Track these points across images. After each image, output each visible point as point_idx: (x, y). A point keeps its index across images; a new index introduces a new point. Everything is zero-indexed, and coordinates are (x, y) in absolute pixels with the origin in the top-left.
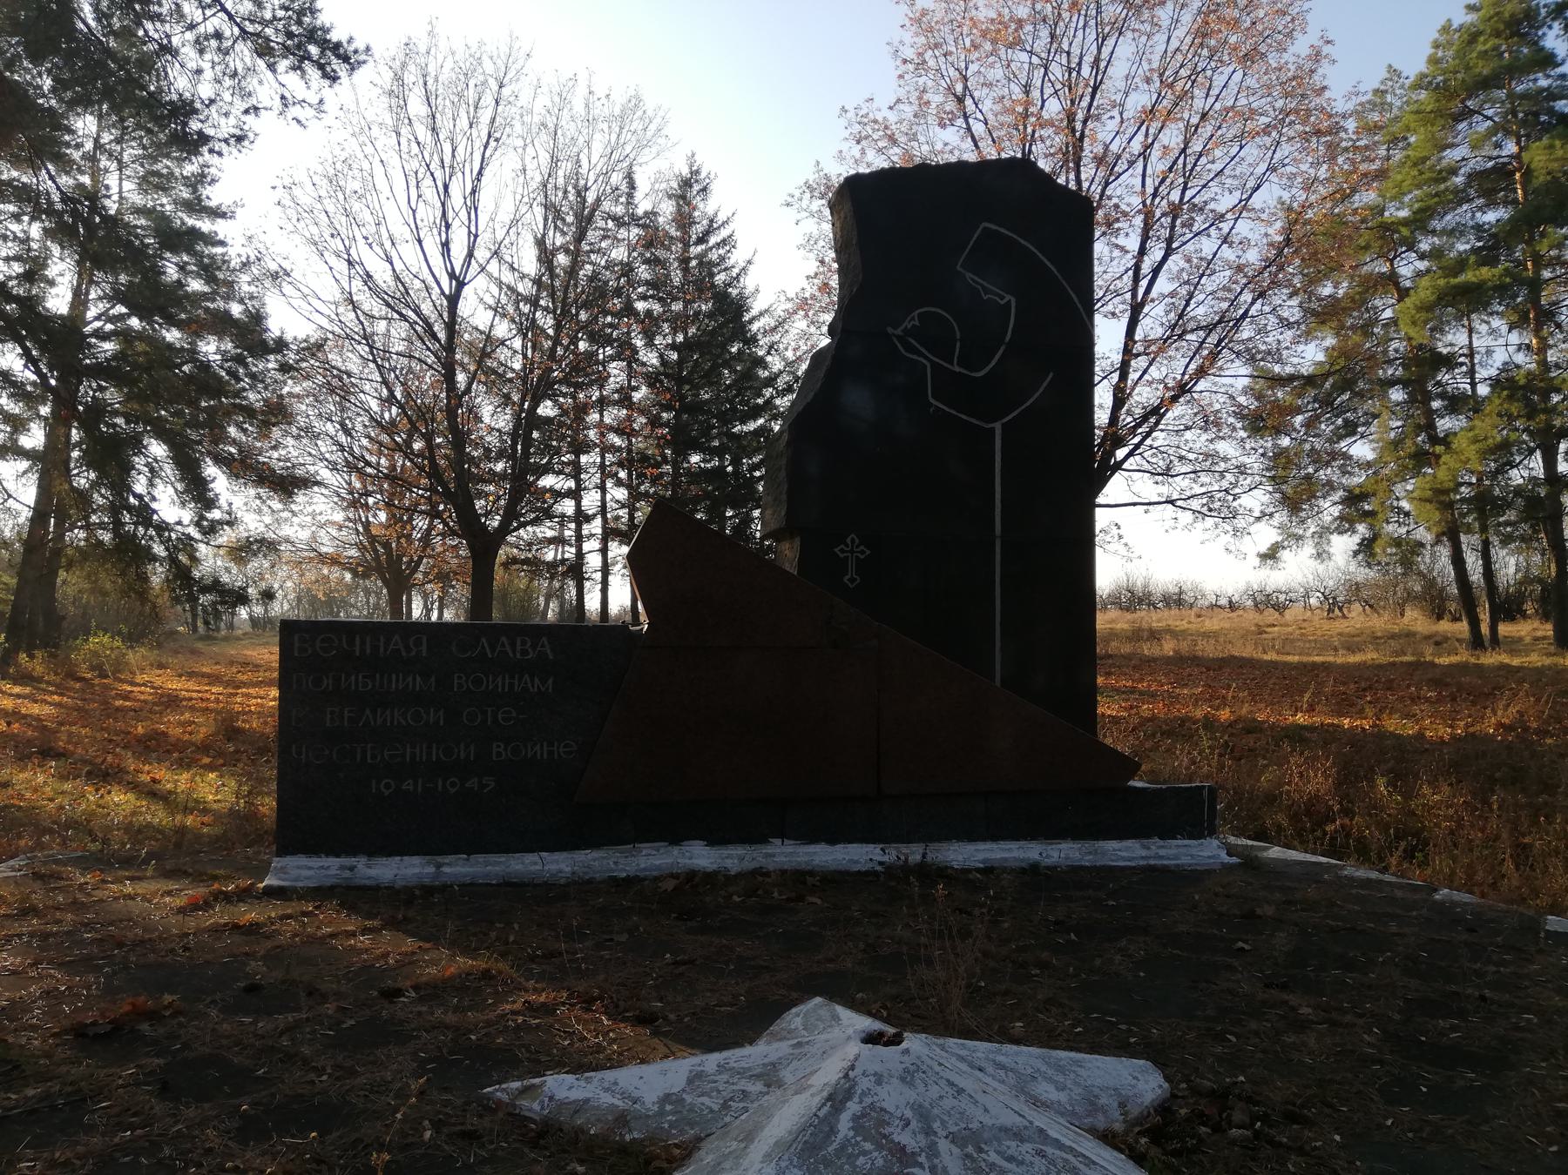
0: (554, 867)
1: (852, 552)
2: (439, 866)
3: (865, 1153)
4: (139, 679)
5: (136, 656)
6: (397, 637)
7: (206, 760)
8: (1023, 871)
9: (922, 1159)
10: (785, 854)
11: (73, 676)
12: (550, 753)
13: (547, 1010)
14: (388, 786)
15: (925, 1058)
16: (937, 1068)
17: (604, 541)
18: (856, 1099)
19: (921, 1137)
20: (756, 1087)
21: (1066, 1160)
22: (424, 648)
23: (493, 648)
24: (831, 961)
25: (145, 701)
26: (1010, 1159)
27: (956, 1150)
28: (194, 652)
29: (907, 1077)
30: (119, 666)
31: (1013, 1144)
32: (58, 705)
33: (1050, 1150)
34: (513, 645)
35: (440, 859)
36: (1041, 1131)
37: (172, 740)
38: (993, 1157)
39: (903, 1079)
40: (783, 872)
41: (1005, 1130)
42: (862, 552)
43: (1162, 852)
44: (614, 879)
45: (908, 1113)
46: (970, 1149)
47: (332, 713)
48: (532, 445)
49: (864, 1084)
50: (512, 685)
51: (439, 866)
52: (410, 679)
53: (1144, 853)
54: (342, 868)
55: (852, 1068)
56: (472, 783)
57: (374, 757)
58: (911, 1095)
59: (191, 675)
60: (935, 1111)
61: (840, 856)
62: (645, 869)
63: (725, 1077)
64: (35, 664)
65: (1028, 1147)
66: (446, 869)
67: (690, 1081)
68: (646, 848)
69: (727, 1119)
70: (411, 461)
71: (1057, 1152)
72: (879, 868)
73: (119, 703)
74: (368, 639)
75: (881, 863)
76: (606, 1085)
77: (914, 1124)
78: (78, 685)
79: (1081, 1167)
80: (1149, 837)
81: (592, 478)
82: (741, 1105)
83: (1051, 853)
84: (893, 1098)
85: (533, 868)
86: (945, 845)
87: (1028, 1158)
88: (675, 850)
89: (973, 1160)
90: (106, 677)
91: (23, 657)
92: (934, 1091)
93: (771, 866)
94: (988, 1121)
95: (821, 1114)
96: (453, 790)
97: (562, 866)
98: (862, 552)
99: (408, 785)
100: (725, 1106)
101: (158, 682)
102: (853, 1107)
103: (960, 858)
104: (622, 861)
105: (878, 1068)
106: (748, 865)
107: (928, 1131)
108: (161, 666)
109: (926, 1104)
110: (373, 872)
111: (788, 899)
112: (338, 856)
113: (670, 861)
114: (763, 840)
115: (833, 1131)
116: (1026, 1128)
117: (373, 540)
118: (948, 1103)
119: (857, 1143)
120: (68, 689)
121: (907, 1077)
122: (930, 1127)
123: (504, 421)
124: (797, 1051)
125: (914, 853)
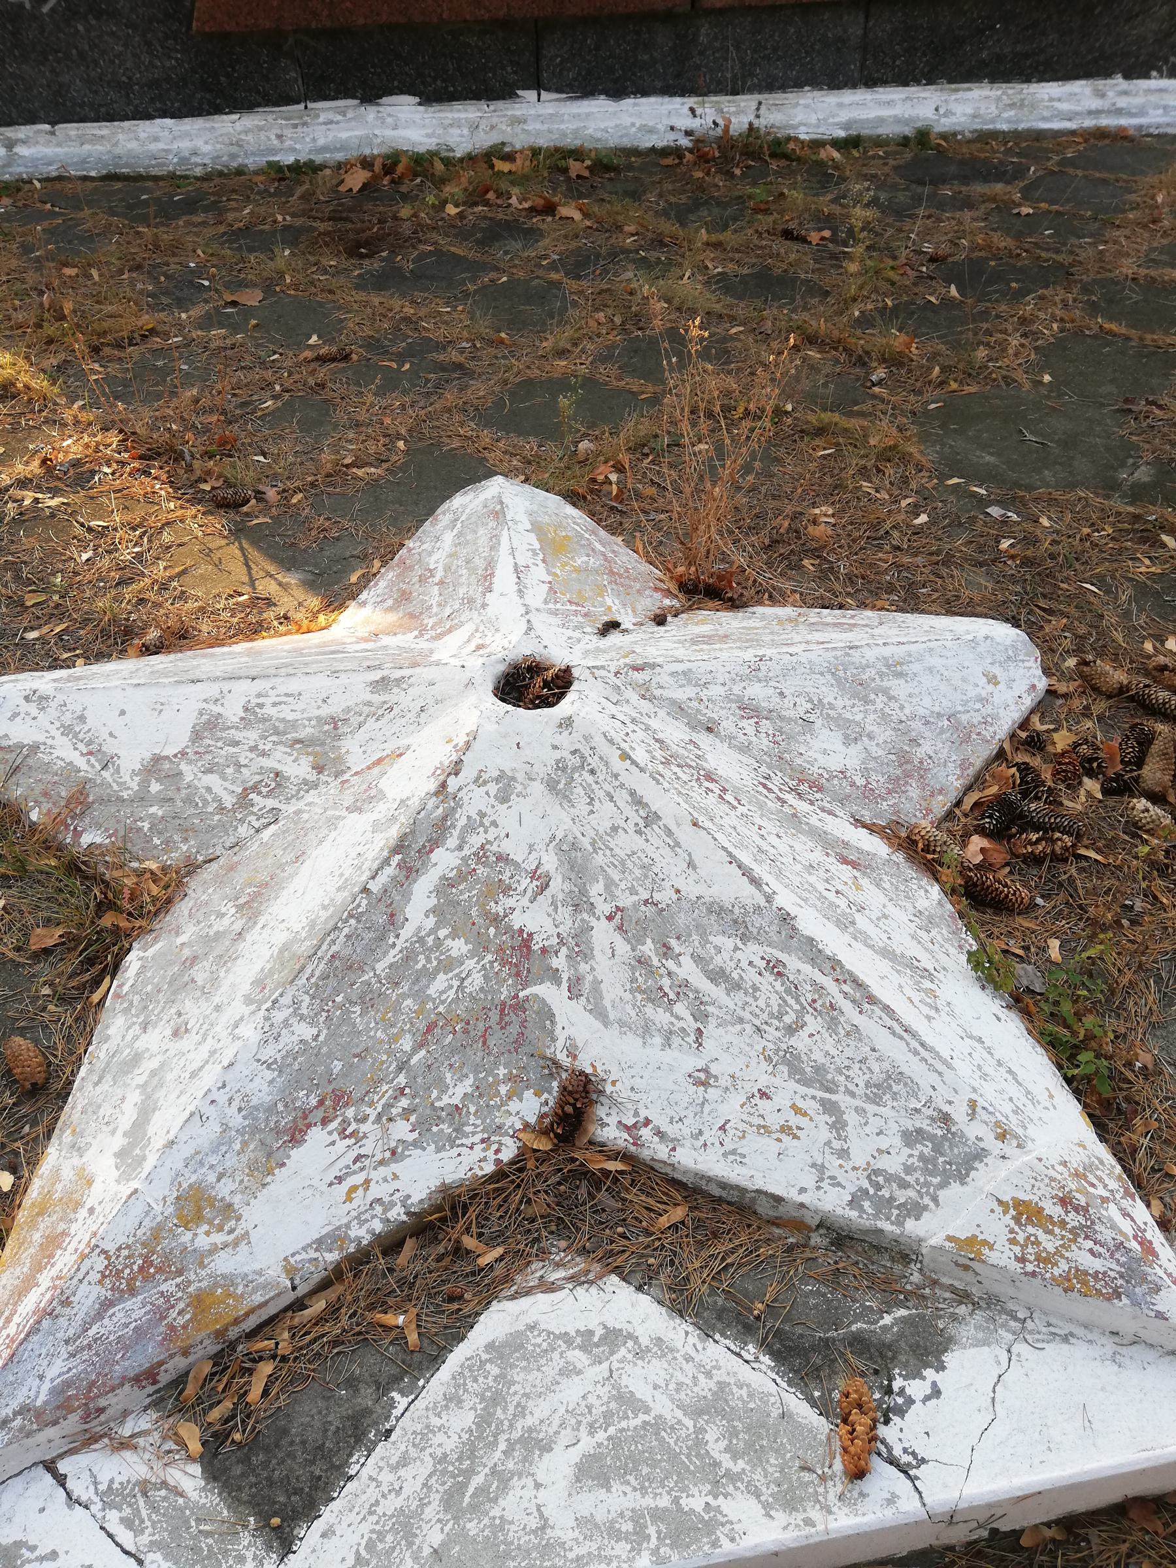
0: (185, 145)
3: (448, 965)
8: (905, 141)
9: (559, 962)
10: (545, 119)
13: (79, 475)
15: (599, 741)
16: (618, 765)
18: (452, 842)
19: (565, 913)
20: (298, 768)
21: (819, 989)
24: (562, 353)
26: (717, 976)
27: (623, 948)
29: (560, 782)
31: (728, 943)
33: (793, 963)
36: (786, 918)
38: (687, 970)
39: (551, 785)
40: (536, 152)
41: (717, 910)
43: (1122, 102)
44: (276, 167)
45: (550, 862)
46: (648, 948)
49: (475, 801)
53: (1095, 104)
55: (456, 768)
58: (561, 820)
60: (599, 859)
61: (626, 120)
62: (324, 149)
63: (251, 736)
65: (753, 952)
66: (21, 150)
67: (197, 736)
68: (325, 110)
69: (243, 831)
71: (807, 969)
72: (685, 142)
75: (688, 133)
76: (68, 719)
77: (557, 885)
79: (846, 1006)
80: (1108, 75)
82: (270, 803)
83: (954, 107)
84: (527, 829)
85: (154, 147)
86: (791, 97)
87: (751, 976)
88: (370, 113)
89: (651, 972)
92: (606, 815)
93: (519, 140)
94: (692, 890)
95: (375, 887)
97: (199, 143)
100: (243, 801)
102: (444, 860)
103: (813, 119)
104: (288, 132)
105: (506, 761)
106: (484, 140)
107: (580, 903)
109: (585, 842)
111: (532, 209)
114: (504, 92)
115: (394, 920)
116: (758, 909)
118: (626, 842)
119: (439, 942)
121: (560, 782)
122: (583, 892)
124: (376, 699)
125: (739, 112)
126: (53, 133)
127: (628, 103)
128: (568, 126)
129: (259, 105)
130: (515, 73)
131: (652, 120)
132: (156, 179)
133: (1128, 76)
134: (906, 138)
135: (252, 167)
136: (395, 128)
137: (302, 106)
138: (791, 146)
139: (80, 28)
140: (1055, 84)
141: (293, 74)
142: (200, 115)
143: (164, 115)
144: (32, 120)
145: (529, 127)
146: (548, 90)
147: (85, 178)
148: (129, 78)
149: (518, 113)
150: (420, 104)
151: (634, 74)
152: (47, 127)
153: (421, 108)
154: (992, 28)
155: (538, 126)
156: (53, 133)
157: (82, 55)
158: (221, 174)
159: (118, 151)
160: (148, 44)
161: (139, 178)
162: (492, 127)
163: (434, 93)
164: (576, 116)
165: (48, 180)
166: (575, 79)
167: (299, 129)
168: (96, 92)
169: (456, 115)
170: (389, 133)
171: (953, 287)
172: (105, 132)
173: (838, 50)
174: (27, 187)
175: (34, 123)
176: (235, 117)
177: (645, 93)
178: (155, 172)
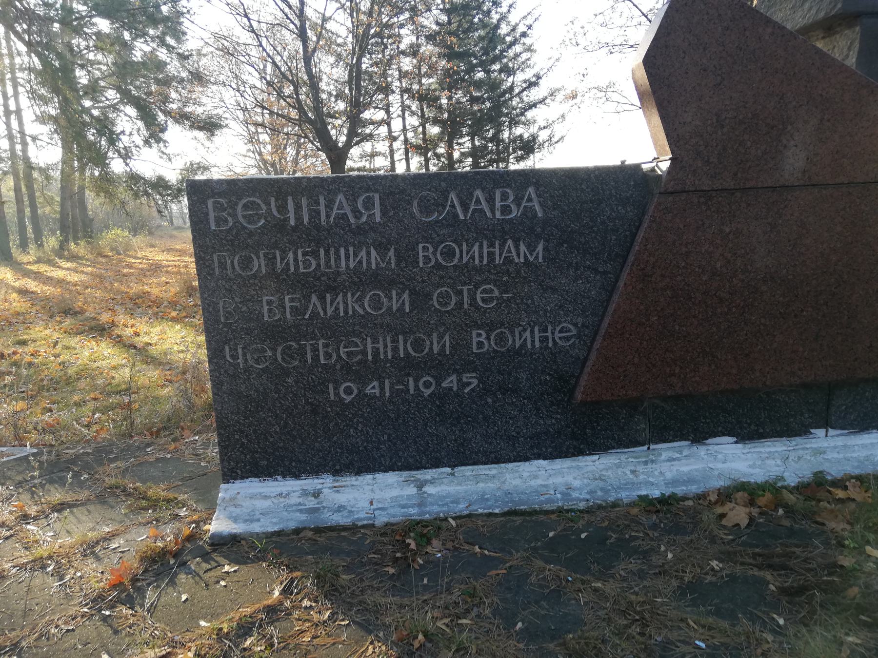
2: (420, 485)
4: (139, 255)
5: (137, 241)
6: (340, 197)
7: (174, 314)
11: (101, 255)
12: (544, 340)
14: (348, 391)
17: (407, 153)
22: (377, 211)
23: (465, 207)
25: (142, 269)
28: (171, 236)
30: (128, 248)
32: (91, 274)
34: (491, 200)
35: (420, 475)
37: (153, 298)
47: (269, 303)
48: (361, 91)
50: (491, 255)
51: (420, 485)
52: (363, 253)
54: (305, 493)
56: (451, 382)
57: (328, 356)
59: (169, 250)
62: (674, 482)
64: (79, 248)
66: (429, 489)
68: (665, 450)
70: (285, 101)
73: (126, 271)
74: (304, 202)
78: (104, 260)
81: (395, 109)
88: (701, 451)
90: (120, 254)
91: (72, 245)
96: (427, 392)
97: (569, 479)
99: (372, 389)
101: (151, 257)
104: (641, 468)
108: (152, 246)
110: (342, 498)
112: (297, 477)
113: (699, 466)
117: (265, 162)
120: (98, 263)
123: (341, 73)
126: (453, 474)
129: (613, 448)
130: (810, 417)
132: (547, 512)
135: (625, 501)
137: (646, 447)
139: (490, 401)
141: (643, 426)
142: (566, 457)
143: (539, 457)
144: (436, 465)
146: (832, 428)
147: (490, 515)
148: (518, 433)
150: (736, 442)
152: (448, 470)
153: (740, 446)
155: (836, 455)
156: (453, 474)
157: (486, 419)
158: (600, 507)
159: (506, 487)
160: (538, 409)
161: (534, 512)
162: (799, 458)
163: (748, 432)
164: (864, 446)
165: (460, 517)
166: (855, 420)
167: (650, 466)
168: (490, 443)
169: (768, 450)
170: (720, 466)
172: (494, 472)
174: (444, 524)
175: (438, 467)
176: (596, 457)
178: (547, 507)
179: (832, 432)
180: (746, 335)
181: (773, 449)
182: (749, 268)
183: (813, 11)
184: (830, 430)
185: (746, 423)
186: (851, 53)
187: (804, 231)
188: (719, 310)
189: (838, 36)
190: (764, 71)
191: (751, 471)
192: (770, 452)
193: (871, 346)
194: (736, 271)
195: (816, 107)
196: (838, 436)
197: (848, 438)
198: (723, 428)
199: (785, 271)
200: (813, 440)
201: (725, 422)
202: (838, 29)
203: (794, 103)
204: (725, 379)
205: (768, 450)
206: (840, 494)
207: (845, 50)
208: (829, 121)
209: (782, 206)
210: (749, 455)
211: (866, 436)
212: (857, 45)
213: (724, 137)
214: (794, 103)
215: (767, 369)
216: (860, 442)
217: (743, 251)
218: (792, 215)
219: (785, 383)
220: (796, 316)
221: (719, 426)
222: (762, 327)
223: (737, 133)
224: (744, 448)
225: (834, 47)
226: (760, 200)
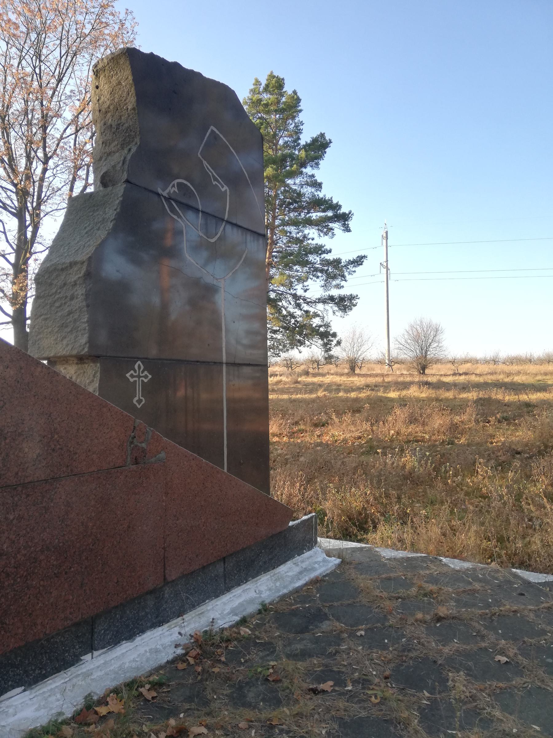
1: (139, 377)
42: (146, 377)
61: (141, 650)
72: (180, 651)
80: (293, 557)
98: (146, 377)
127: (138, 640)
128: (115, 666)
130: (80, 648)
131: (154, 647)
133: (299, 555)
134: (259, 610)
136: (15, 715)
138: (226, 633)
140: (282, 566)
145: (95, 676)
146: (96, 650)
149: (84, 670)
150: (24, 691)
151: (138, 624)
153: (27, 693)
154: (261, 553)
155: (99, 673)
164: (117, 658)
166: (110, 639)
169: (49, 688)
170: (11, 720)
171: (425, 691)
173: (216, 580)
177: (143, 631)
179: (96, 653)
180: (29, 598)
181: (53, 686)
182: (30, 544)
183: (70, 347)
184: (94, 652)
185: (32, 670)
186: (95, 379)
187: (69, 509)
188: (6, 583)
189: (86, 366)
190: (37, 397)
191: (38, 714)
192: (52, 689)
193: (118, 582)
194: (20, 549)
195: (74, 421)
196: (100, 655)
197: (107, 654)
198: (12, 681)
199: (57, 541)
200: (83, 666)
201: (14, 675)
202: (86, 361)
203: (59, 419)
204: (13, 640)
205: (49, 688)
206: (103, 710)
207: (91, 376)
208: (83, 430)
209: (53, 493)
210: (35, 699)
211: (118, 649)
212: (98, 374)
213: (7, 446)
214: (59, 419)
215: (46, 621)
216: (114, 656)
217: (24, 532)
218: (60, 498)
219: (60, 628)
220: (66, 573)
221: (9, 681)
222: (41, 588)
223: (17, 443)
224: (30, 694)
225: (84, 372)
226: (36, 490)
